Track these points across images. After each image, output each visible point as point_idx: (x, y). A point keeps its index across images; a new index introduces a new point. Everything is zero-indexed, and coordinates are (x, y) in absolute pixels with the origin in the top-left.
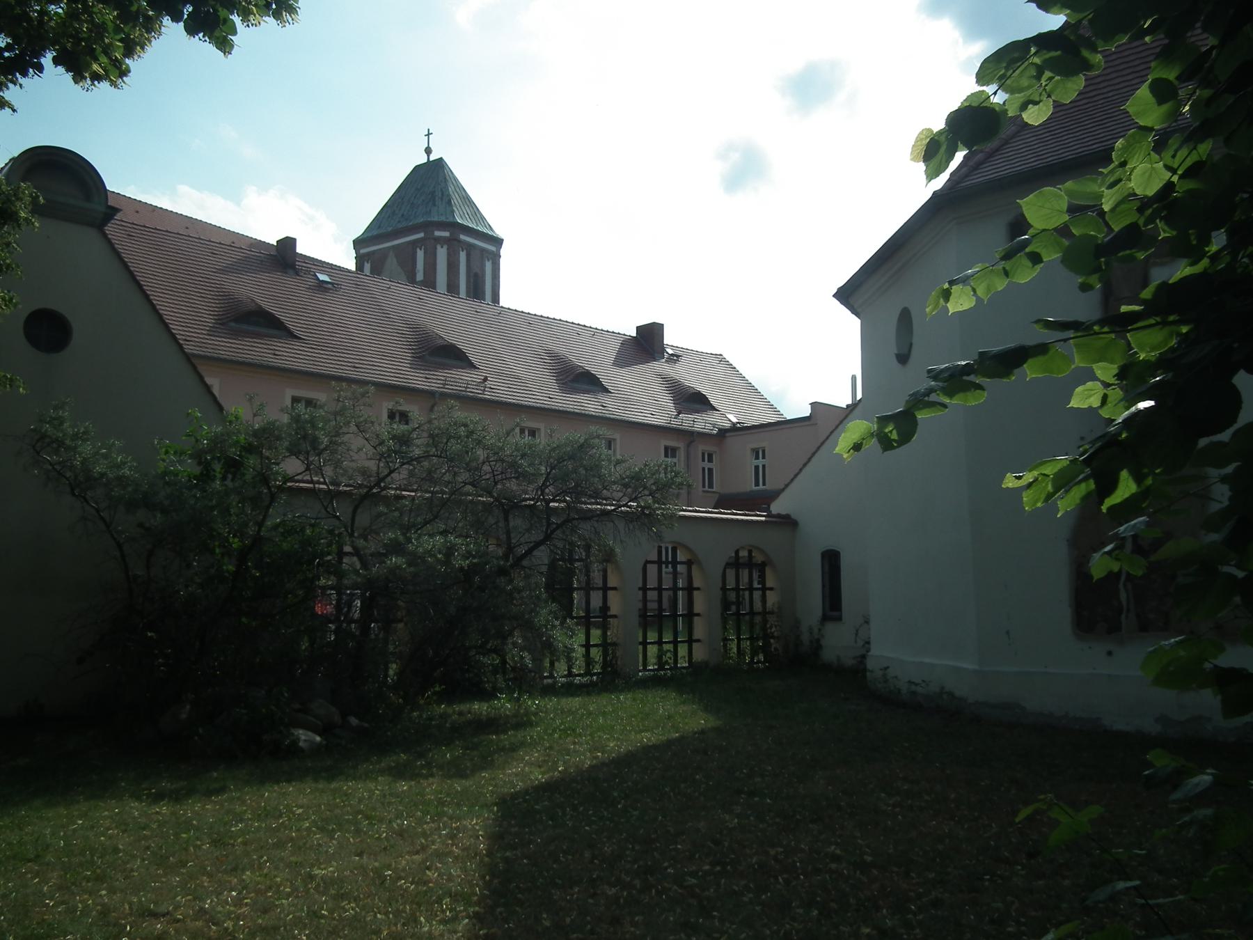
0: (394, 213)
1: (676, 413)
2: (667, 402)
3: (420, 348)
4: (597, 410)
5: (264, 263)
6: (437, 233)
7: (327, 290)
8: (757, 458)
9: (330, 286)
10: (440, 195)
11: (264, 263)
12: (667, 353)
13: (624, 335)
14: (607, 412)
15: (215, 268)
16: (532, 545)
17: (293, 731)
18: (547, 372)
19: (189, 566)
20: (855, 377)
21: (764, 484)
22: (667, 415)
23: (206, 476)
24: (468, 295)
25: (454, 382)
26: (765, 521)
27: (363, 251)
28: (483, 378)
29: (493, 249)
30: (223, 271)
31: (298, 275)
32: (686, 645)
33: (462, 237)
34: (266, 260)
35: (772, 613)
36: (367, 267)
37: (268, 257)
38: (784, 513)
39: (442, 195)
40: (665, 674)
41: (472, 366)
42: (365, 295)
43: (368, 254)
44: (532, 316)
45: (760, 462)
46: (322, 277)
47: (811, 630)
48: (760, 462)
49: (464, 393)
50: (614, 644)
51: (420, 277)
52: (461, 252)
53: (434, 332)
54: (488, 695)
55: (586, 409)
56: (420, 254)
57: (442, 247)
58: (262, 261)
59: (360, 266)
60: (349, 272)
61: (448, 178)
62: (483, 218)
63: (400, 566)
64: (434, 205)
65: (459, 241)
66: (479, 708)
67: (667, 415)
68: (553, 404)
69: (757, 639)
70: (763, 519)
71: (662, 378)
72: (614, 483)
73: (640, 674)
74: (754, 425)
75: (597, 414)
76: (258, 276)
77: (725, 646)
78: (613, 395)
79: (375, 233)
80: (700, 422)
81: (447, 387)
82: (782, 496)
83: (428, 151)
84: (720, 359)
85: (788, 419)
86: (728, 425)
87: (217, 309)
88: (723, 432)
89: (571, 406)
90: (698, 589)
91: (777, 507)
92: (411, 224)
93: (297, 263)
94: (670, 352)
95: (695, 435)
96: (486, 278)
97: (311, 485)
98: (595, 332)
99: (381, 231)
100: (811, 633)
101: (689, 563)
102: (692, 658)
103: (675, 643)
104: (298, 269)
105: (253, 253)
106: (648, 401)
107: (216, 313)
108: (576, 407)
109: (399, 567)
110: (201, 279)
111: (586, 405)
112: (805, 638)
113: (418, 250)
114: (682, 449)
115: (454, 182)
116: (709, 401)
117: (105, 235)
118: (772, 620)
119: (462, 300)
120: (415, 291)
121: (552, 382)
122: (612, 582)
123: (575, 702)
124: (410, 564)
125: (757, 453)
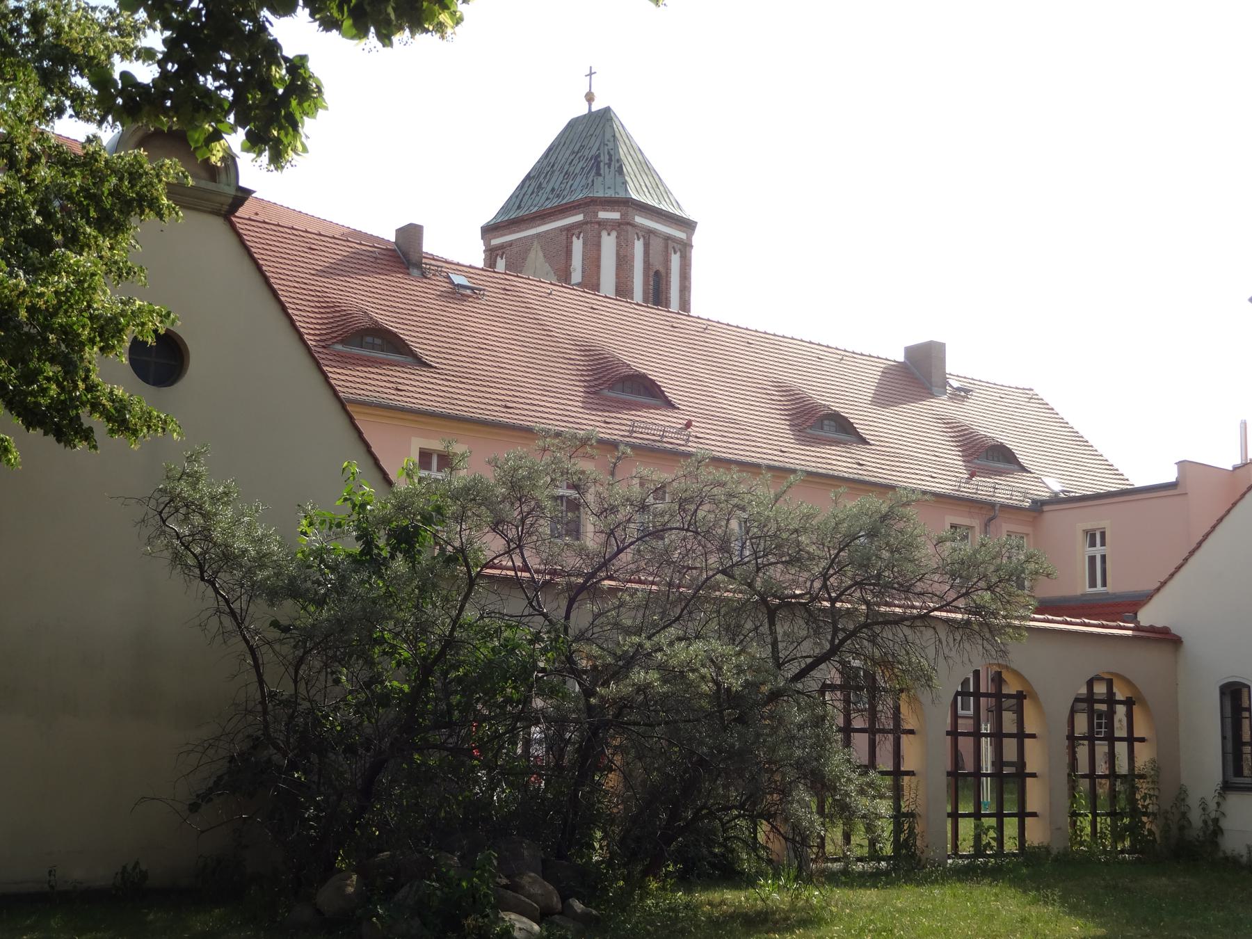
0: (540, 187)
1: (966, 476)
2: (954, 459)
3: (596, 379)
4: (850, 470)
5: (378, 261)
6: (603, 215)
7: (464, 298)
8: (1093, 544)
9: (469, 292)
10: (607, 161)
11: (378, 261)
12: (951, 386)
13: (886, 359)
14: (865, 473)
15: (314, 269)
16: (809, 660)
17: (502, 914)
18: (776, 414)
19: (337, 682)
20: (1245, 424)
21: (1104, 584)
22: (955, 479)
23: (368, 559)
24: (646, 300)
25: (646, 428)
26: (1134, 637)
27: (496, 242)
28: (685, 422)
29: (681, 235)
30: (324, 273)
31: (426, 278)
32: (1016, 820)
33: (639, 220)
34: (382, 257)
35: (1142, 777)
36: (501, 265)
37: (390, 253)
38: (1159, 624)
39: (610, 159)
40: (986, 863)
41: (670, 405)
42: (679, 339)
43: (502, 247)
44: (743, 331)
45: (1098, 551)
46: (458, 279)
47: (1204, 807)
48: (1098, 551)
49: (659, 444)
50: (911, 815)
51: (576, 277)
52: (636, 241)
53: (614, 357)
54: (748, 881)
55: (834, 468)
56: (577, 245)
57: (609, 234)
58: (376, 258)
59: (491, 261)
60: (434, 259)
61: (617, 135)
62: (667, 192)
63: (650, 683)
64: (598, 174)
65: (634, 225)
66: (734, 898)
67: (955, 479)
68: (787, 460)
69: (1122, 815)
70: (1129, 633)
71: (944, 423)
72: (934, 571)
73: (950, 861)
74: (1084, 495)
75: (851, 476)
76: (371, 279)
77: (1074, 824)
78: (873, 447)
79: (513, 215)
80: (1005, 489)
81: (635, 435)
82: (1156, 600)
83: (590, 98)
84: (1031, 396)
85: (1136, 486)
86: (1045, 495)
87: (318, 327)
88: (1039, 506)
89: (814, 464)
90: (1033, 736)
91: (1148, 616)
92: (564, 202)
93: (424, 260)
94: (955, 384)
95: (997, 508)
96: (672, 279)
97: (513, 573)
98: (844, 356)
99: (521, 213)
100: (1204, 809)
101: (1020, 696)
102: (1025, 842)
103: (1000, 816)
104: (425, 268)
105: (364, 248)
106: (926, 456)
107: (317, 332)
108: (819, 465)
109: (649, 685)
110: (296, 285)
111: (834, 462)
112: (1196, 817)
113: (574, 238)
114: (977, 529)
115: (627, 141)
116: (663, 392)
117: (233, 226)
118: (1143, 787)
119: (672, 315)
120: (586, 297)
121: (783, 427)
122: (909, 721)
123: (870, 896)
124: (665, 681)
125: (1093, 537)
